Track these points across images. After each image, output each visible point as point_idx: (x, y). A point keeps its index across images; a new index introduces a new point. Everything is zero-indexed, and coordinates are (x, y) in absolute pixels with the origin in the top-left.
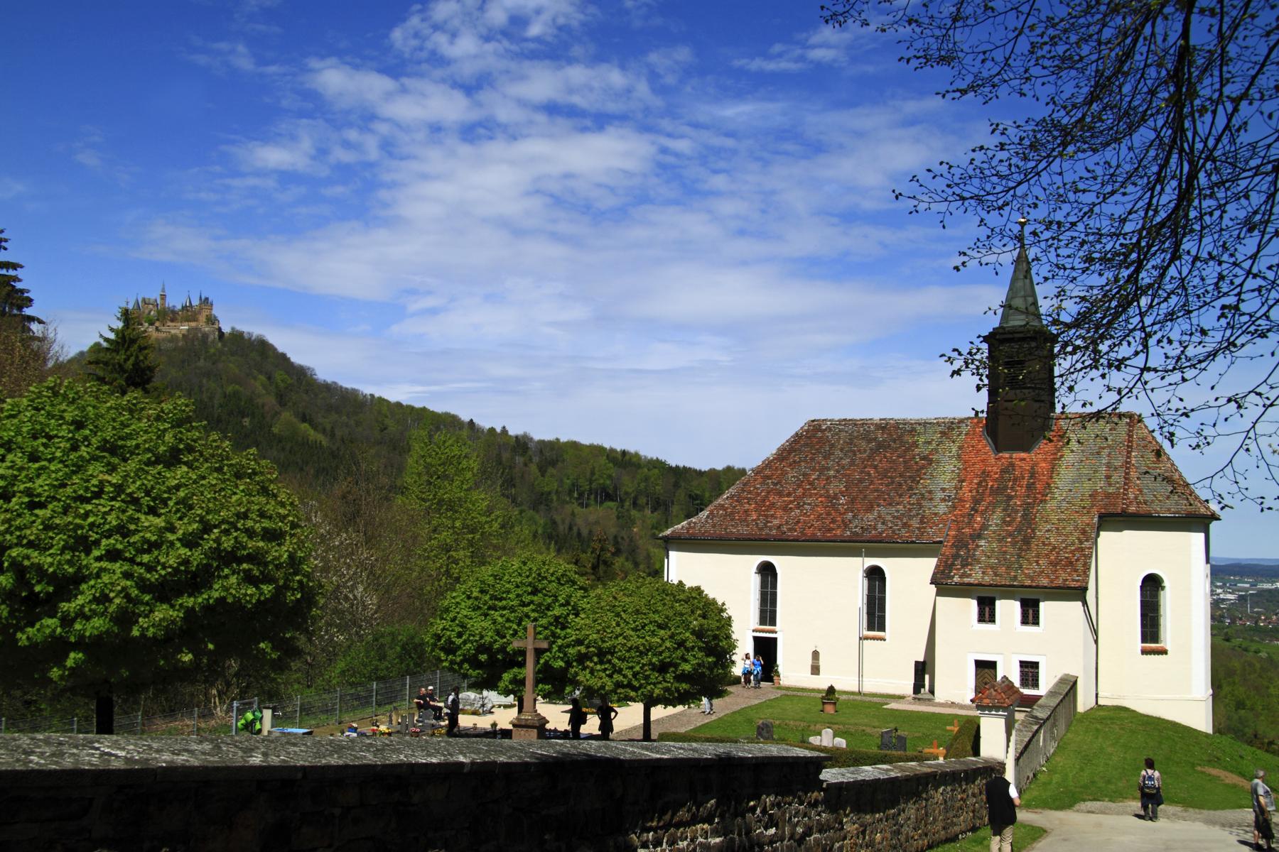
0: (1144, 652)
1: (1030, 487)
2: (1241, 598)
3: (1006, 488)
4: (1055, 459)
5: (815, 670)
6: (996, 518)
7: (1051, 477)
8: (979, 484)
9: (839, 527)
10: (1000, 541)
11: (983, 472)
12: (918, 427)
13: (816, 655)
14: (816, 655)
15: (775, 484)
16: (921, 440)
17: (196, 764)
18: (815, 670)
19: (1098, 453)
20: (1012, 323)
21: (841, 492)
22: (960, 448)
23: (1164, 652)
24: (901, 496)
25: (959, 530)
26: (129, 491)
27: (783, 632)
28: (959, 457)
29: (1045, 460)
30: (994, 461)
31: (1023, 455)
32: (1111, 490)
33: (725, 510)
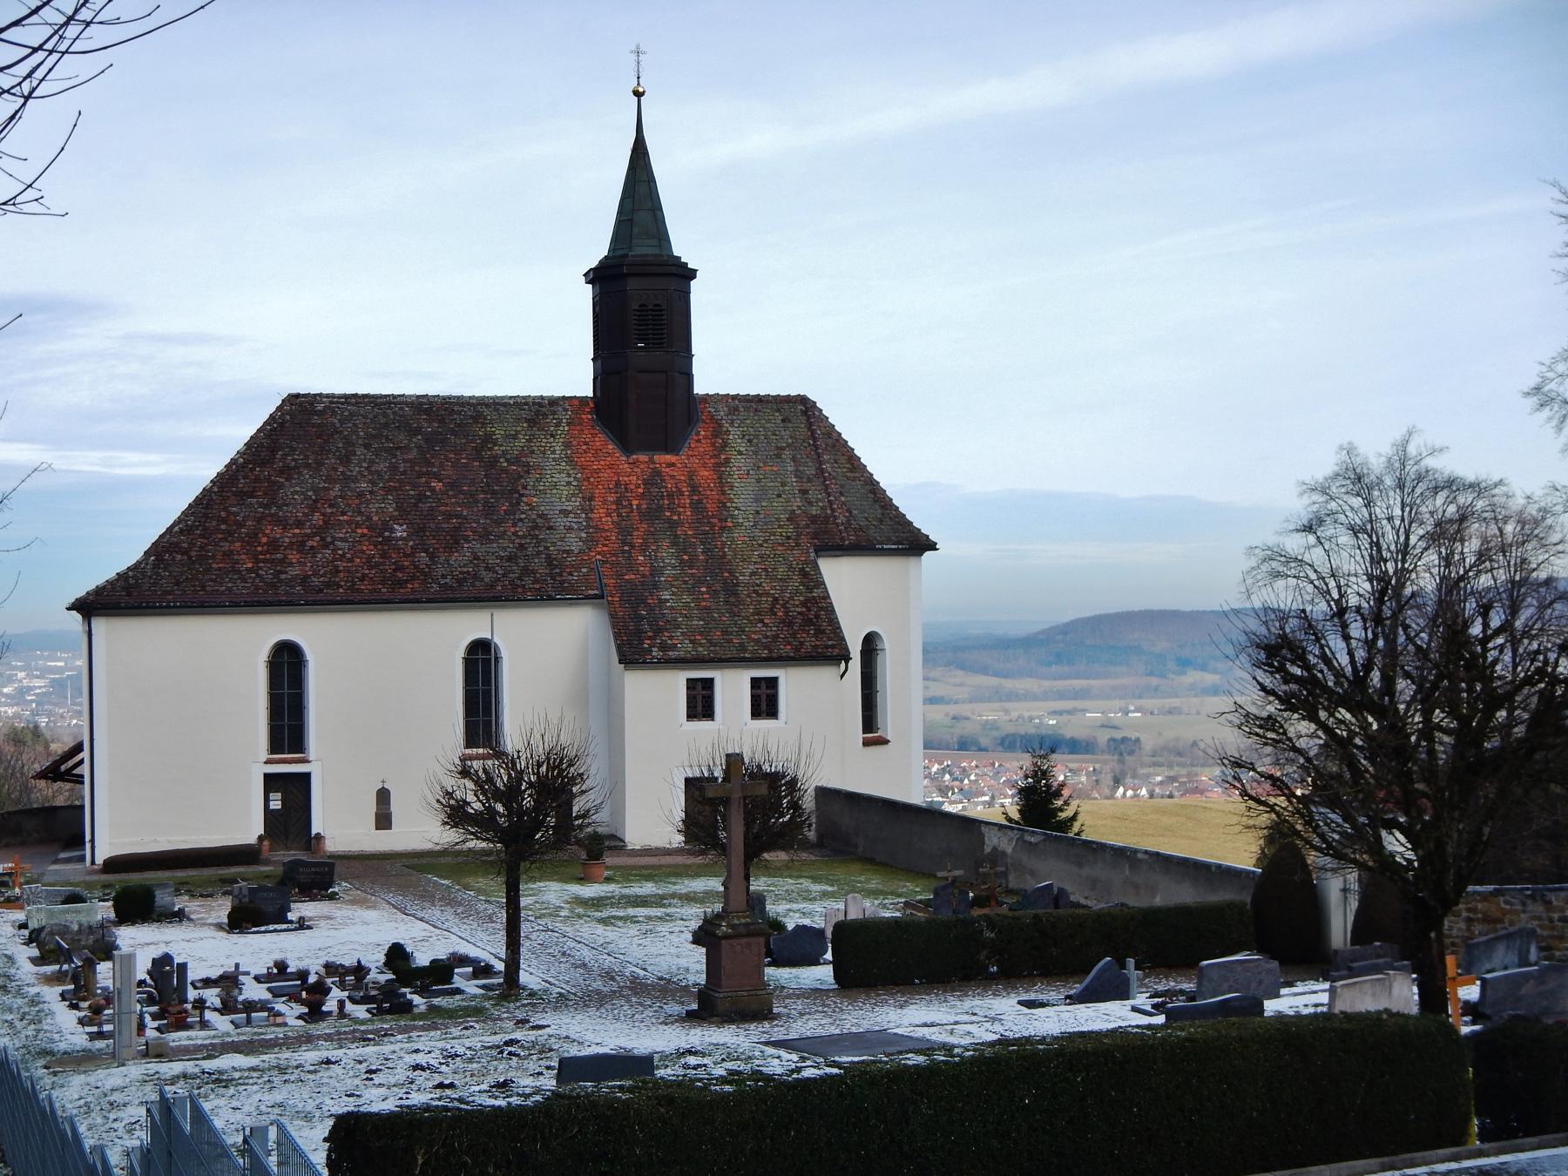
0: (867, 743)
1: (697, 506)
2: (54, 682)
3: (660, 508)
4: (719, 465)
5: (383, 820)
6: (667, 555)
7: (724, 493)
8: (618, 502)
9: (414, 578)
10: (691, 591)
11: (618, 484)
12: (486, 412)
13: (383, 796)
14: (383, 796)
15: (266, 506)
16: (499, 434)
17: (1096, 905)
18: (383, 820)
19: (778, 456)
20: (638, 251)
21: (394, 519)
22: (567, 445)
23: (886, 742)
24: (499, 523)
25: (620, 576)
26: (1391, 571)
27: (322, 759)
28: (570, 460)
29: (704, 465)
30: (632, 468)
31: (669, 458)
32: (814, 511)
33: (185, 552)
